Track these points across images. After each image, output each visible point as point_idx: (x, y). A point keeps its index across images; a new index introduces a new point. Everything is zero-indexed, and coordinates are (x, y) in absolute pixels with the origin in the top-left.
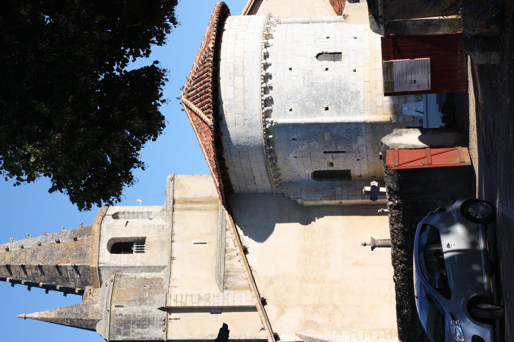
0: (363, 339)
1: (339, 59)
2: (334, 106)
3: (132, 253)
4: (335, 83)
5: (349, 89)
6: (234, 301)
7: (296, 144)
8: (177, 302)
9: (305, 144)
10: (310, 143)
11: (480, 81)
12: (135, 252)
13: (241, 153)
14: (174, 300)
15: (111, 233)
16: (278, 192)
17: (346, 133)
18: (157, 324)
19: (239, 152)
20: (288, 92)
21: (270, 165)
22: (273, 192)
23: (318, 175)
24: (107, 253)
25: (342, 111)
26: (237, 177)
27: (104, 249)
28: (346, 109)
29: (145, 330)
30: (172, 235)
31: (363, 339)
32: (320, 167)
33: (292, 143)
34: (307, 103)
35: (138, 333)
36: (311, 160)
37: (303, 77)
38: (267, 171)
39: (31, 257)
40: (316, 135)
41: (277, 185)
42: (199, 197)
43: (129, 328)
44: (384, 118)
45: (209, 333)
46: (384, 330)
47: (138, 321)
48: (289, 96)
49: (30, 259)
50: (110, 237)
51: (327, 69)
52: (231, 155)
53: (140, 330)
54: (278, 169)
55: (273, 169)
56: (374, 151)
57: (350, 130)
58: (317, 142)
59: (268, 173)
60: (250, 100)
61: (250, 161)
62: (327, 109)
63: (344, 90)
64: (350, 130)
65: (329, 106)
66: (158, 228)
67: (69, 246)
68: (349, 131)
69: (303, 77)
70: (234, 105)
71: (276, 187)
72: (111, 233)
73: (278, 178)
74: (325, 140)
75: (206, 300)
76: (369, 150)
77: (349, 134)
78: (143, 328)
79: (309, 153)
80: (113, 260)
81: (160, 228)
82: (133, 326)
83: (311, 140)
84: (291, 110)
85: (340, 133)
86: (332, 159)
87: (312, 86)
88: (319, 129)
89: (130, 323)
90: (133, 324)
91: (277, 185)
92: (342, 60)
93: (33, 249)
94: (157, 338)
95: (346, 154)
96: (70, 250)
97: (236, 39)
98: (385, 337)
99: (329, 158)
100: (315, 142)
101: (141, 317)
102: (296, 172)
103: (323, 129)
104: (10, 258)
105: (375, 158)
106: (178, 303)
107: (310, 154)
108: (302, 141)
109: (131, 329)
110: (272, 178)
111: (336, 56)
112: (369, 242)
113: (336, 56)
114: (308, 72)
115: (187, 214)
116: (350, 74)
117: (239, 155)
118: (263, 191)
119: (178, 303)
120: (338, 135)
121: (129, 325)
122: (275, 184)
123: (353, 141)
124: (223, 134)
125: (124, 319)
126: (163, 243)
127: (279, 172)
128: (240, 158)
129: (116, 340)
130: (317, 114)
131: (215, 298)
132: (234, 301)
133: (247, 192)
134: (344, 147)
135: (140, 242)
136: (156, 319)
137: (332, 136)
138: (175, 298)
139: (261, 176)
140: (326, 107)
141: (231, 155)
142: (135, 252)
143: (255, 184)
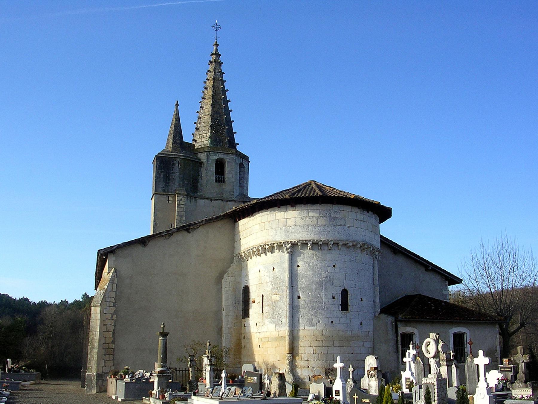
0: (104, 324)
7: (270, 271)
9: (270, 278)
10: (270, 283)
11: (383, 241)
13: (264, 224)
17: (278, 313)
19: (264, 223)
23: (246, 290)
24: (216, 158)
26: (246, 224)
27: (218, 156)
30: (227, 201)
31: (104, 324)
33: (271, 267)
36: (257, 284)
45: (158, 223)
46: (113, 342)
47: (168, 175)
51: (334, 298)
52: (262, 216)
55: (252, 251)
56: (263, 338)
57: (281, 318)
58: (271, 289)
61: (257, 232)
64: (281, 318)
74: (273, 296)
76: (264, 334)
77: (277, 317)
79: (262, 282)
81: (232, 193)
83: (273, 283)
85: (278, 309)
88: (282, 291)
92: (342, 311)
95: (261, 314)
97: (361, 221)
98: (105, 343)
99: (259, 300)
100: (271, 287)
103: (282, 294)
105: (258, 338)
107: (262, 283)
108: (272, 275)
116: (329, 318)
117: (262, 223)
118: (235, 246)
120: (277, 307)
123: (271, 320)
124: (279, 209)
126: (222, 194)
128: (259, 224)
134: (267, 313)
135: (223, 180)
136: (169, 187)
137: (276, 302)
138: (182, 200)
139: (246, 243)
141: (262, 216)
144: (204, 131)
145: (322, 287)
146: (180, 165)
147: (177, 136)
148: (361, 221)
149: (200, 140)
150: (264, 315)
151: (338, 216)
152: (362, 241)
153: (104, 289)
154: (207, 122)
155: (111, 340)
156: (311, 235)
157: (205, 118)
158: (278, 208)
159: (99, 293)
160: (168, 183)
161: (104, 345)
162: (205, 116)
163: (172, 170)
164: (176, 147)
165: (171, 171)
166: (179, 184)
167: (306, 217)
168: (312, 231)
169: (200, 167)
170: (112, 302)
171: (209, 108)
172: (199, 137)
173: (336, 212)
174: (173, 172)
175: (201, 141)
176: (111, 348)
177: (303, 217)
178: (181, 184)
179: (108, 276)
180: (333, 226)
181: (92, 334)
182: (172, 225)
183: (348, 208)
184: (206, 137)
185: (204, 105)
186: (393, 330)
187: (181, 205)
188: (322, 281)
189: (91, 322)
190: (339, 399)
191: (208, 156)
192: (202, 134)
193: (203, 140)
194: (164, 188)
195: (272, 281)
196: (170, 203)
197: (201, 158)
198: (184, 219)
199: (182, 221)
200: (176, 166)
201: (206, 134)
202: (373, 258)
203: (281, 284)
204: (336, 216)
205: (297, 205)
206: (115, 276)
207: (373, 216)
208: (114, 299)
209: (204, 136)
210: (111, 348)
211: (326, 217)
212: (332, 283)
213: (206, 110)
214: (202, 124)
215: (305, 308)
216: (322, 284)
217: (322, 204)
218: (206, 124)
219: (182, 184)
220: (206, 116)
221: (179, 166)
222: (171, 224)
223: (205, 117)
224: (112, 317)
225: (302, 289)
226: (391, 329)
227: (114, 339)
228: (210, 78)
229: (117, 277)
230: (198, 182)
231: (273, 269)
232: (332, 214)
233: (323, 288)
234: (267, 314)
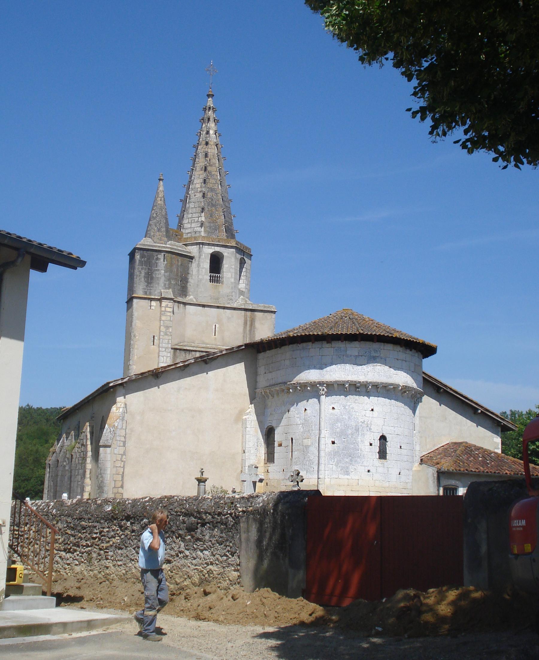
1: (380, 458)
2: (336, 450)
3: (210, 273)
4: (358, 452)
5: (351, 465)
6: (163, 356)
8: (165, 307)
12: (211, 275)
14: (168, 305)
15: (228, 255)
16: (256, 394)
17: (310, 460)
18: (148, 289)
20: (351, 406)
21: (282, 388)
22: (257, 390)
25: (330, 458)
27: (214, 249)
28: (333, 461)
29: (143, 279)
32: (279, 433)
34: (339, 424)
35: (141, 273)
37: (364, 421)
38: (277, 384)
39: (211, 188)
40: (309, 431)
41: (263, 394)
42: (256, 332)
43: (145, 266)
44: (377, 430)
45: (137, 334)
46: (122, 487)
48: (347, 407)
49: (210, 187)
50: (225, 254)
51: (371, 445)
53: (143, 274)
54: (279, 394)
59: (274, 385)
60: (344, 370)
61: (287, 368)
62: (333, 443)
63: (351, 460)
65: (335, 445)
66: (231, 296)
67: (219, 219)
68: (311, 463)
69: (364, 421)
70: (340, 355)
71: (261, 393)
72: (228, 255)
73: (270, 395)
74: (304, 440)
75: (166, 333)
78: (145, 277)
80: (205, 256)
81: (230, 297)
82: (147, 269)
84: (333, 408)
85: (309, 454)
86: (285, 446)
87: (355, 430)
89: (149, 266)
90: (149, 269)
91: (263, 394)
92: (380, 460)
93: (218, 190)
94: (135, 288)
96: (215, 221)
97: (403, 360)
98: (115, 487)
101: (154, 276)
102: (275, 411)
104: (212, 170)
106: (164, 308)
109: (145, 267)
110: (270, 389)
111: (383, 454)
112: (205, 476)
113: (383, 454)
114: (369, 427)
115: (241, 321)
119: (164, 308)
120: (308, 452)
121: (148, 266)
122: (264, 392)
124: (313, 344)
125: (153, 261)
126: (218, 299)
127: (275, 396)
128: (290, 359)
129: (136, 254)
130: (329, 433)
131: (167, 340)
132: (163, 356)
133: (258, 366)
136: (152, 289)
138: (169, 306)
140: (335, 442)
142: (211, 275)
143: (265, 373)
144: (194, 214)
145: (359, 433)
146: (165, 260)
147: (162, 221)
148: (403, 360)
149: (189, 226)
150: (293, 461)
151: (378, 355)
152: (403, 383)
153: (114, 426)
154: (198, 202)
155: (120, 484)
156: (348, 375)
157: (196, 196)
158: (312, 343)
159: (109, 430)
160: (151, 283)
161: (114, 489)
162: (196, 194)
163: (155, 266)
164: (160, 236)
165: (155, 268)
166: (165, 285)
167: (343, 355)
168: (350, 371)
169: (190, 263)
170: (122, 441)
171: (201, 183)
172: (187, 222)
173: (376, 351)
174: (156, 268)
175: (191, 227)
176: (120, 493)
177: (340, 355)
178: (167, 285)
179: (117, 411)
180: (373, 366)
181: (101, 477)
182: (155, 337)
183: (390, 347)
184: (197, 222)
185: (194, 178)
186: (434, 482)
187: (167, 313)
188: (359, 426)
189: (100, 463)
190: (511, 411)
191: (201, 249)
192: (192, 218)
193: (193, 225)
194: (145, 289)
195: (303, 424)
196: (153, 309)
197: (192, 250)
198: (171, 331)
199: (169, 333)
200: (161, 262)
201: (197, 218)
202: (415, 401)
203: (314, 427)
204: (377, 355)
205: (334, 341)
206: (125, 412)
207: (416, 355)
208: (123, 437)
209: (194, 220)
210: (120, 493)
211: (365, 356)
212: (370, 428)
213: (197, 185)
214: (192, 205)
215: (340, 454)
216: (359, 429)
217: (361, 342)
218: (197, 205)
219: (168, 285)
220: (197, 193)
221: (164, 261)
222: (154, 336)
223: (196, 195)
224: (121, 459)
225: (337, 434)
226: (432, 481)
227: (123, 483)
228: (203, 141)
229: (127, 413)
230: (187, 282)
231: (304, 409)
232: (371, 353)
233: (360, 434)
234: (296, 459)
